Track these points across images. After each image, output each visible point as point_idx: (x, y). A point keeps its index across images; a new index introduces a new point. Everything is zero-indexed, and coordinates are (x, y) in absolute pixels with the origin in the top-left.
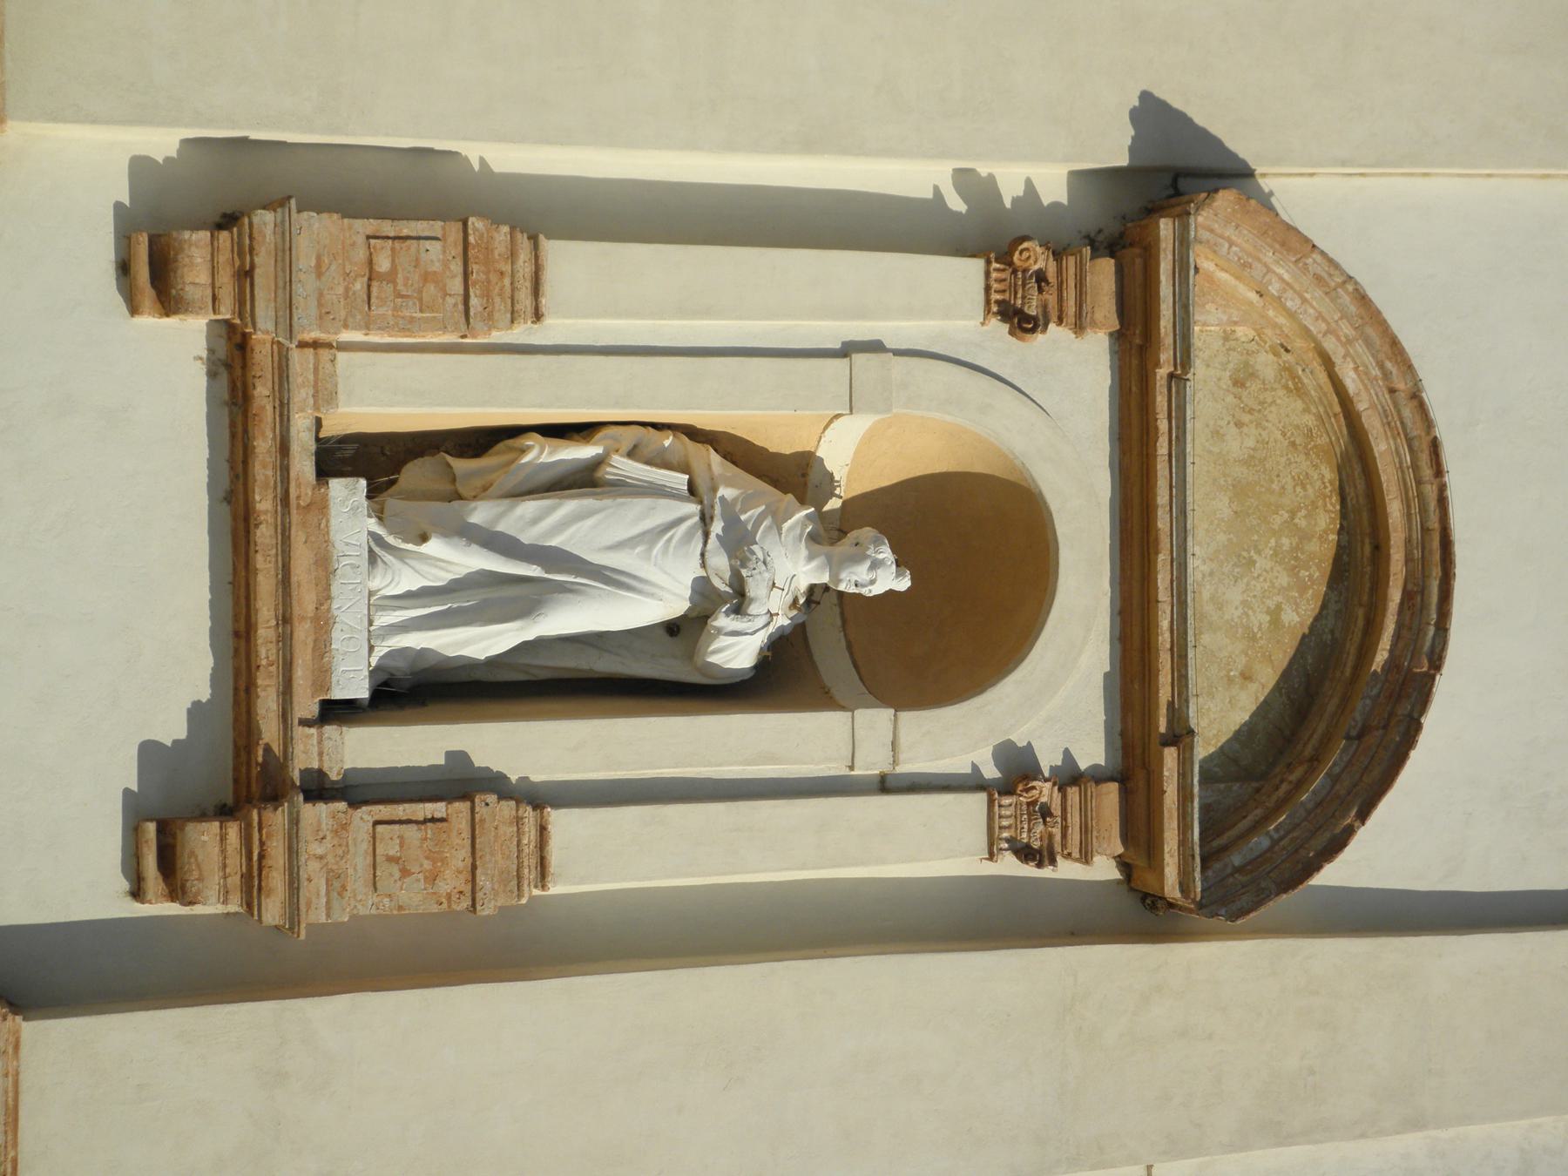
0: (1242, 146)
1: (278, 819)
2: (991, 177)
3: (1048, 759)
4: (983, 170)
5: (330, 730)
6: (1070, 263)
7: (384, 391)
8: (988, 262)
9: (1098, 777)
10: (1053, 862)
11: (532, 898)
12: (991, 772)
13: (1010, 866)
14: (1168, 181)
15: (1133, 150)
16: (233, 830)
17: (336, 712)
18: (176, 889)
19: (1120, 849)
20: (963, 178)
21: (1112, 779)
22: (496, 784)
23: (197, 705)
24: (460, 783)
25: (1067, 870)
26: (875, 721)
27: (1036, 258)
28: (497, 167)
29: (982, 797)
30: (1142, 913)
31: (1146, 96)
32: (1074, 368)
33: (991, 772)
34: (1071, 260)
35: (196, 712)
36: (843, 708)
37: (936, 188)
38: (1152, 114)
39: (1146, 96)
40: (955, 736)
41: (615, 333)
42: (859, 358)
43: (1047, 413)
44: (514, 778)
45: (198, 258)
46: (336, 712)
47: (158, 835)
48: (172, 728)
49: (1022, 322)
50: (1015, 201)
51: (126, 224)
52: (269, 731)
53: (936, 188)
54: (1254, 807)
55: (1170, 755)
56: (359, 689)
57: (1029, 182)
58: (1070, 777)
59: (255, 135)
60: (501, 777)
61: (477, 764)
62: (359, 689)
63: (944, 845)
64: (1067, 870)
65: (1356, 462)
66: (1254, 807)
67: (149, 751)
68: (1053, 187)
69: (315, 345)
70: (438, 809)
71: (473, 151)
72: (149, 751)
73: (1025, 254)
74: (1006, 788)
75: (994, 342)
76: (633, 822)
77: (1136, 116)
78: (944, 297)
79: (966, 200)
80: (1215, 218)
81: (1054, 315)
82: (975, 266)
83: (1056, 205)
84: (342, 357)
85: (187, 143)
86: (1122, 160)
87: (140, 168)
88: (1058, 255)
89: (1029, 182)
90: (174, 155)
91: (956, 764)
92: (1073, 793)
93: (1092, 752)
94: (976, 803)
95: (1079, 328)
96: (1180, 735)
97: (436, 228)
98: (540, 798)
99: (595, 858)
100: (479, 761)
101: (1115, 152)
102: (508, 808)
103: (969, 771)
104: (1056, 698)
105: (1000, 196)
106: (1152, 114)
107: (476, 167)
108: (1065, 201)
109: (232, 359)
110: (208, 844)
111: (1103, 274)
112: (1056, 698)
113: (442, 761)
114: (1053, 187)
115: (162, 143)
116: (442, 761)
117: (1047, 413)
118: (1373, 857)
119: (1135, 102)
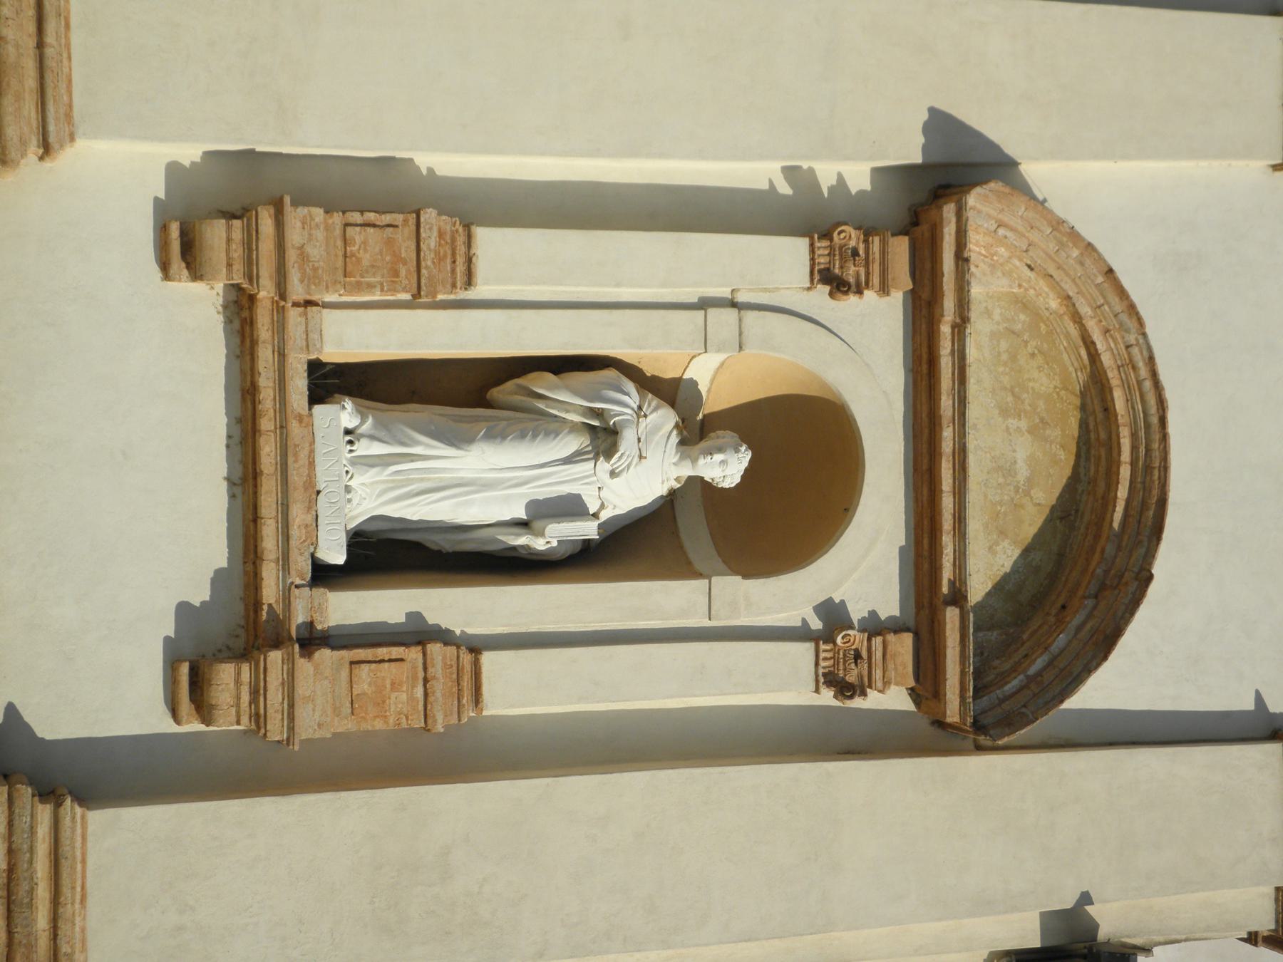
0: (1011, 150)
1: (275, 656)
2: (811, 170)
3: (857, 613)
4: (805, 165)
5: (319, 592)
6: (876, 242)
7: (357, 336)
8: (812, 239)
9: (896, 627)
10: (864, 694)
11: (470, 718)
12: (816, 624)
13: (827, 697)
14: (947, 176)
15: (925, 149)
16: (245, 669)
17: (323, 575)
18: (203, 709)
19: (912, 683)
20: (790, 172)
21: (908, 630)
22: (443, 636)
23: (218, 572)
24: (418, 634)
25: (873, 701)
26: (730, 586)
27: (850, 236)
28: (441, 171)
29: (809, 646)
30: (930, 734)
31: (933, 111)
32: (877, 319)
33: (816, 624)
34: (877, 239)
35: (219, 578)
36: (697, 575)
37: (771, 182)
38: (941, 125)
39: (933, 111)
40: (788, 597)
41: (522, 294)
42: (713, 313)
43: (857, 354)
44: (458, 632)
45: (216, 235)
46: (323, 575)
47: (190, 673)
48: (200, 594)
49: (838, 285)
50: (831, 189)
51: (163, 214)
52: (270, 593)
53: (771, 182)
54: (1017, 649)
55: (952, 614)
56: (336, 556)
57: (840, 175)
58: (875, 627)
59: (259, 149)
60: (448, 632)
61: (430, 622)
62: (336, 556)
63: (785, 681)
64: (873, 701)
65: (1097, 385)
66: (1017, 649)
67: (184, 610)
68: (859, 178)
69: (309, 303)
70: (396, 652)
71: (425, 160)
72: (184, 610)
73: (842, 235)
74: (827, 636)
75: (819, 300)
76: (550, 658)
77: (927, 129)
78: (783, 262)
79: (792, 187)
80: (981, 203)
81: (876, 280)
82: (802, 244)
83: (862, 193)
84: (325, 311)
85: (208, 155)
86: (918, 159)
87: (174, 171)
88: (868, 233)
89: (840, 175)
90: (198, 160)
91: (788, 618)
92: (878, 641)
93: (889, 605)
94: (804, 651)
95: (884, 290)
96: (958, 597)
97: (398, 218)
98: (476, 647)
99: (518, 690)
100: (431, 620)
101: (909, 149)
102: (451, 650)
103: (799, 624)
104: (863, 567)
105: (818, 186)
106: (941, 125)
107: (424, 172)
108: (868, 187)
109: (240, 309)
110: (228, 680)
111: (900, 248)
112: (863, 567)
113: (403, 620)
114: (859, 178)
115: (189, 153)
116: (403, 620)
117: (857, 354)
118: (1102, 691)
119: (925, 116)
